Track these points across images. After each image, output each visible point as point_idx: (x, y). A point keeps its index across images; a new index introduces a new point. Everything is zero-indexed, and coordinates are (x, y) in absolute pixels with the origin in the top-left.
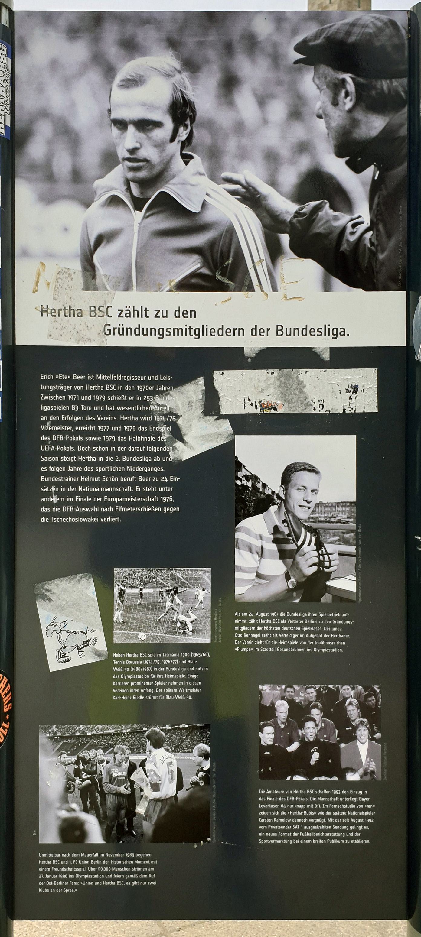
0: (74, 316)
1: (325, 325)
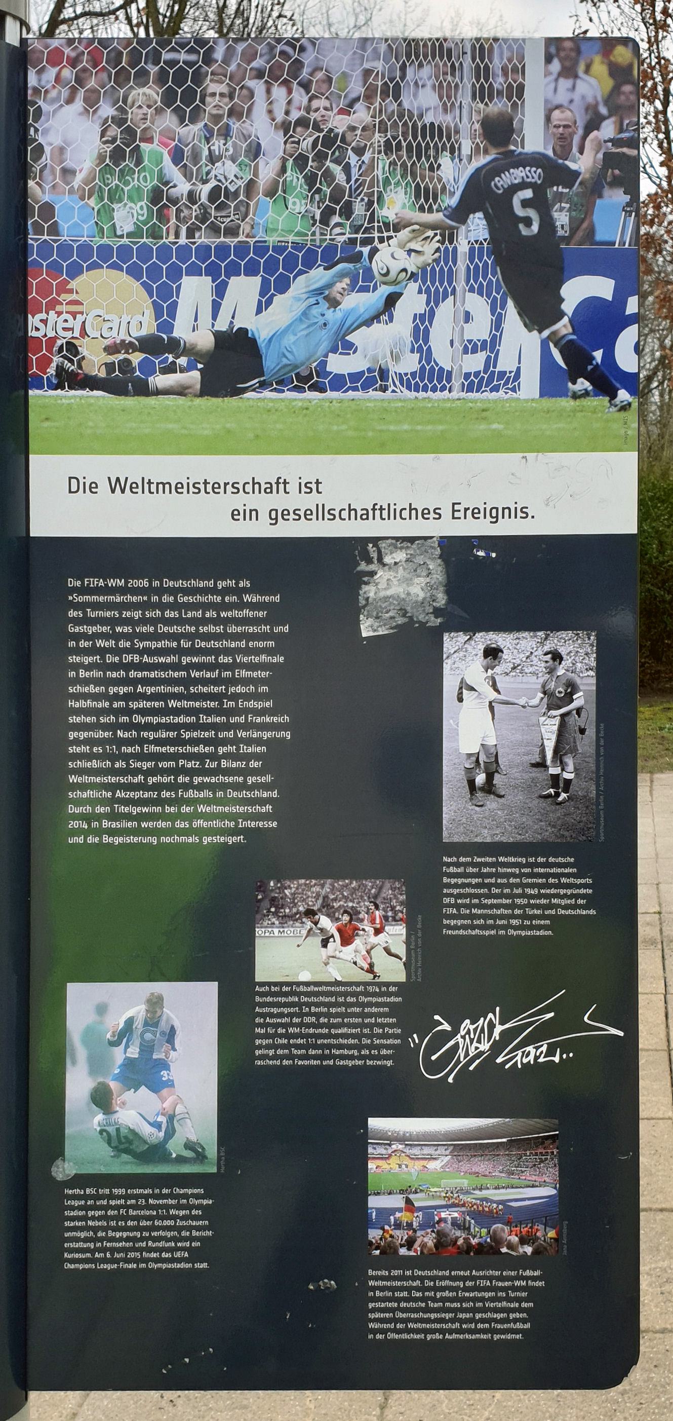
0: (356, 519)
1: (389, 505)
